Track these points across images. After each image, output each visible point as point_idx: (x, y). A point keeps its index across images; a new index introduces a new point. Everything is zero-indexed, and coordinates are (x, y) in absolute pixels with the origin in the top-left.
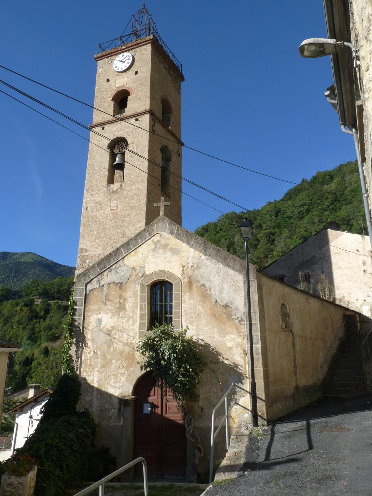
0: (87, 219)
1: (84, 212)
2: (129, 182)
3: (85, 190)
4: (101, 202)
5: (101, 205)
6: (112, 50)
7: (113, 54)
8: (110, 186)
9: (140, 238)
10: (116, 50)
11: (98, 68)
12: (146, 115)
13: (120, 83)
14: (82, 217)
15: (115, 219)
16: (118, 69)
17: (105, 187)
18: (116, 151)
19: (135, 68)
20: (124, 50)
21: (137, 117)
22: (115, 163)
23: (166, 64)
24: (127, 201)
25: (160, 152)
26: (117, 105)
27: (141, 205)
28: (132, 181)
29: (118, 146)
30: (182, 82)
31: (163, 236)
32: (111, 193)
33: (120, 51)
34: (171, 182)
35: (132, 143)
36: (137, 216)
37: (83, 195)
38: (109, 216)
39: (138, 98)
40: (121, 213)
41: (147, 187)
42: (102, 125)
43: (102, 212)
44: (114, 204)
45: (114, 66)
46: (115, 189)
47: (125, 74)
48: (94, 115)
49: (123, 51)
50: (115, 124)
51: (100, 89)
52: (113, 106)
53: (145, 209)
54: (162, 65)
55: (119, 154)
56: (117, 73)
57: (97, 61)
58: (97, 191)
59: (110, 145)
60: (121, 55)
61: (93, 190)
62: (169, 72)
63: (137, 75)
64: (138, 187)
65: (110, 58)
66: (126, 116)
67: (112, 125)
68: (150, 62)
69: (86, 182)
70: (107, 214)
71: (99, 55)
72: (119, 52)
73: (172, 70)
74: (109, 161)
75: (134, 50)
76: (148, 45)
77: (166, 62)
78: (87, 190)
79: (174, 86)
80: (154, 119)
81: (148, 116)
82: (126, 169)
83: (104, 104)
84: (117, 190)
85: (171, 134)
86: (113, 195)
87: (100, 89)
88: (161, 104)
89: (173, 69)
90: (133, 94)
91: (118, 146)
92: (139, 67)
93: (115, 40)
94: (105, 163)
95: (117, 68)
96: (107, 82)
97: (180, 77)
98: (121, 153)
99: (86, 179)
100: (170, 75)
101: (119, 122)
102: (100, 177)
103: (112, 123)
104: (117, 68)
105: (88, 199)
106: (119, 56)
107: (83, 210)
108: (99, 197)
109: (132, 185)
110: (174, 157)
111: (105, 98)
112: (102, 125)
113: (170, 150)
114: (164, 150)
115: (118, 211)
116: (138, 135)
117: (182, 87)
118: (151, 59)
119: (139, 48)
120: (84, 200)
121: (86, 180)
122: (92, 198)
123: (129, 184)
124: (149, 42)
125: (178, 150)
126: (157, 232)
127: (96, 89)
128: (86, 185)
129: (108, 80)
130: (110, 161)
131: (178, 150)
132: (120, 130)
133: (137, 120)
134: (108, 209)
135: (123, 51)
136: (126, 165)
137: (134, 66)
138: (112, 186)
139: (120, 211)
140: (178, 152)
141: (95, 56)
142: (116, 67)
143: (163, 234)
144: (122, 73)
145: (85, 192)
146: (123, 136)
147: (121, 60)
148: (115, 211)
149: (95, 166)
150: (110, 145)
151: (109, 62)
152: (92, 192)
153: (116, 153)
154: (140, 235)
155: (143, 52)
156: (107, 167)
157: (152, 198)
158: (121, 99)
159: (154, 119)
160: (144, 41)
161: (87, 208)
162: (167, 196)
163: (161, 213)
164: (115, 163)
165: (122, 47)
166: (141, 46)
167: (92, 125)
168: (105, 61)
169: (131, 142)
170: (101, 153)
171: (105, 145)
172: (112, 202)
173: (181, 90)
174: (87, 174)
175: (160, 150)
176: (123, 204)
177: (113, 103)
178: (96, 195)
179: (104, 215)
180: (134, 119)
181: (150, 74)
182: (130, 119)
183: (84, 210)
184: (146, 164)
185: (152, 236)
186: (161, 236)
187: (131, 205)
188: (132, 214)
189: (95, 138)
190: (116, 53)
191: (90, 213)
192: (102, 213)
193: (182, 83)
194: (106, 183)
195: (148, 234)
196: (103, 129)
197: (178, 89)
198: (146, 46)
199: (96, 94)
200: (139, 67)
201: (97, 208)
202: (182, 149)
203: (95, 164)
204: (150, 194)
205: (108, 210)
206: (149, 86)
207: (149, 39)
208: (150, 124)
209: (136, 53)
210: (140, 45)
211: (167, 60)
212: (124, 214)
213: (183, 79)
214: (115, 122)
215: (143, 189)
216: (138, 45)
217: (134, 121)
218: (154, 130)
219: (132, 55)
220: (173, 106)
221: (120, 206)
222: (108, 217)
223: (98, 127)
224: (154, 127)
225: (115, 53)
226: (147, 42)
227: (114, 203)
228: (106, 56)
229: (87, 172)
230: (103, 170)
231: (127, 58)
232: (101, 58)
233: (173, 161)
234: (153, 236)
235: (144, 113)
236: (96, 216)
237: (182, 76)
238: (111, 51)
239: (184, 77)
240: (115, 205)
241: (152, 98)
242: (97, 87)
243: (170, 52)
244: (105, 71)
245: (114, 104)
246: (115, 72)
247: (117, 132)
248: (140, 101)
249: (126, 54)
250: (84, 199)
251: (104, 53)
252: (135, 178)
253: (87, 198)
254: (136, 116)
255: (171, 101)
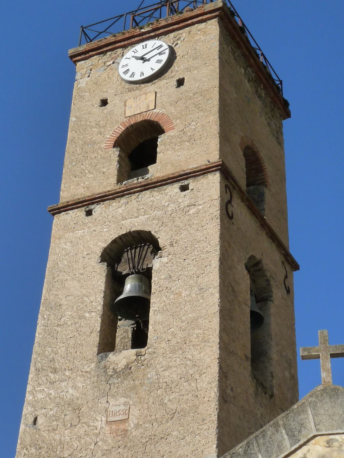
0: (33, 450)
1: (25, 430)
2: (163, 345)
3: (32, 369)
4: (79, 402)
5: (77, 409)
6: (115, 36)
7: (119, 44)
8: (106, 356)
9: (263, 449)
10: (127, 35)
11: (78, 76)
12: (210, 176)
13: (138, 106)
14: (18, 447)
15: (120, 450)
16: (133, 75)
17: (91, 361)
18: (123, 268)
19: (178, 70)
20: (148, 35)
21: (186, 182)
22: (122, 297)
23: (250, 70)
24: (158, 396)
25: (246, 272)
26: (127, 160)
27: (201, 407)
28: (174, 342)
29: (130, 255)
30: (284, 119)
31: (336, 444)
32: (109, 376)
33: (137, 39)
34: (274, 354)
35: (172, 245)
36: (188, 439)
37: (27, 384)
38: (102, 440)
39: (184, 138)
40: (141, 430)
41: (217, 356)
42: (87, 204)
43: (81, 430)
44: (117, 405)
45: (121, 70)
46: (122, 364)
47: (151, 87)
48: (63, 181)
49: (144, 36)
50: (123, 200)
51: (83, 123)
52: (117, 159)
53: (215, 418)
54: (243, 71)
55: (132, 273)
56: (127, 86)
57: (75, 62)
58: (67, 373)
59: (108, 254)
60: (139, 47)
61: (55, 371)
62: (257, 92)
63: (182, 87)
64: (190, 357)
65: (109, 53)
66: (154, 180)
67: (114, 204)
68: (217, 57)
69: (36, 348)
70: (97, 435)
71: (82, 49)
72: (133, 40)
73: (262, 87)
74: (105, 292)
75: (172, 35)
76: (209, 22)
77: (251, 66)
78: (38, 370)
79: (269, 125)
80: (231, 187)
81: (215, 178)
82: (155, 311)
83: (93, 156)
84: (128, 367)
85: (267, 234)
86: (116, 381)
87: (83, 123)
88: (243, 158)
89: (264, 86)
90: (173, 128)
91: (130, 255)
92: (188, 70)
93: (122, 16)
94: (92, 299)
95: (130, 74)
96: (101, 106)
97: (282, 108)
98: (138, 273)
99: (36, 340)
100: (260, 97)
101: (134, 197)
102: (76, 334)
103: (113, 199)
104: (130, 74)
105: (40, 396)
106: (133, 49)
107: (22, 427)
108: (74, 387)
109: (173, 351)
110: (278, 293)
111: (94, 143)
112: (87, 204)
113: (268, 275)
114: (254, 268)
115: (131, 424)
116: (188, 225)
117: (284, 130)
118: (220, 51)
119: (187, 29)
120: (29, 397)
121: (36, 345)
122: (51, 391)
123: (162, 351)
124: (214, 14)
125: (286, 277)
126: (317, 430)
127: (71, 124)
128: (34, 356)
129: (104, 103)
130: (108, 292)
131: (286, 277)
132: (136, 215)
133: (184, 188)
134: (100, 422)
135: (143, 38)
136: (154, 301)
137: (175, 66)
138: (112, 357)
139: (137, 426)
140: (286, 282)
141: (71, 51)
142: (126, 72)
143: (337, 437)
144: (143, 85)
145: (31, 376)
146: (147, 229)
147: (139, 55)
148: (122, 427)
149: (64, 307)
150: (108, 254)
151: (108, 64)
152: (52, 376)
153: (124, 273)
154: (261, 441)
155: (197, 38)
156: (100, 308)
157: (232, 389)
158: (139, 146)
159: (231, 187)
160: (199, 12)
161: (36, 420)
162: (265, 393)
163: (323, 375)
164: (122, 297)
165: (141, 28)
166: (193, 24)
167: (60, 205)
168: (96, 61)
169: (167, 243)
170: (81, 272)
171: (93, 252)
172: (112, 401)
173: (284, 137)
174: (39, 329)
175: (247, 267)
176: (146, 406)
177: (117, 153)
178: (64, 384)
179: (88, 439)
180: (176, 186)
181: (217, 82)
182: (165, 187)
183: (26, 425)
184: (212, 294)
185: (301, 442)
186: (329, 444)
187: (172, 406)
188: (175, 433)
189: (67, 236)
190: (126, 42)
191: (45, 434)
192: (82, 431)
193: (286, 123)
194: (96, 349)
195: (286, 437)
196: (89, 213)
197: (277, 132)
198: (205, 23)
199: (70, 135)
200: (188, 70)
201: (68, 418)
202: (293, 276)
203: (64, 302)
204: (226, 377)
205: (98, 424)
206: (216, 109)
207: (212, 9)
208: (221, 196)
209: (178, 39)
210: (190, 22)
211: (252, 61)
212: (147, 434)
213: (288, 115)
214: (122, 196)
215: (208, 360)
216: (184, 23)
217: (178, 190)
218: (230, 213)
219: (169, 46)
220: (269, 168)
221: (135, 412)
222: (100, 443)
223: (76, 210)
224: (229, 206)
225: (122, 43)
226: (208, 16)
227: (117, 403)
228: (100, 50)
229: (40, 321)
230: (87, 315)
231: (156, 52)
232: (86, 55)
233: (276, 302)
234: (305, 444)
235: (204, 171)
236: (61, 443)
237: (286, 104)
238: (113, 39)
239: (290, 108)
240: (122, 407)
241: (225, 137)
242: (72, 119)
243: (258, 48)
244: (96, 83)
245: (119, 156)
246: (124, 83)
247: (129, 221)
248: (193, 139)
249: (151, 44)
250: (27, 395)
251: (94, 44)
252: (180, 334)
253: (38, 393)
254: (182, 179)
255: (263, 154)
